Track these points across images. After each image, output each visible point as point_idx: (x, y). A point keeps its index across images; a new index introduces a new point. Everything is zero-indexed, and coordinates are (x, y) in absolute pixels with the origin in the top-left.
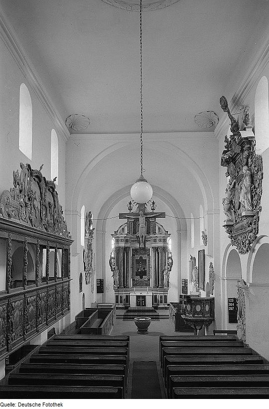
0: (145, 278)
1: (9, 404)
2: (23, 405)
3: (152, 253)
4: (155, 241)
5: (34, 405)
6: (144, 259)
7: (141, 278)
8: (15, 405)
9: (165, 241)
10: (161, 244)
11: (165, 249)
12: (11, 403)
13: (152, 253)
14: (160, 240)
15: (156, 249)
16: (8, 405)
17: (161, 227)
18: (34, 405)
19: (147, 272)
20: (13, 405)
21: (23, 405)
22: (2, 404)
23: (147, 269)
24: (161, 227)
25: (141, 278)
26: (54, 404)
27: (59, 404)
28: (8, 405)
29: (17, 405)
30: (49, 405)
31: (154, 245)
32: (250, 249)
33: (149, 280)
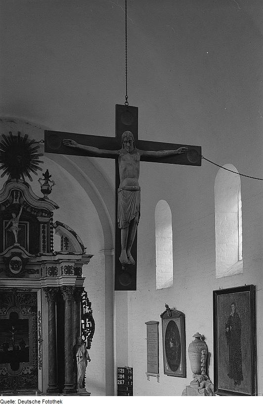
0: (25, 368)
1: (8, 401)
2: (23, 402)
3: (43, 306)
5: (33, 402)
6: (22, 317)
7: (15, 367)
8: (15, 402)
9: (78, 272)
11: (77, 292)
12: (11, 400)
13: (43, 306)
14: (68, 270)
15: (56, 295)
16: (8, 402)
17: (71, 236)
18: (33, 402)
19: (30, 352)
20: (13, 402)
21: (23, 402)
22: (2, 401)
23: (30, 345)
24: (71, 236)
26: (54, 401)
27: (58, 401)
28: (8, 402)
29: (17, 402)
30: (48, 402)
31: (48, 282)
32: (56, 267)
33: (35, 372)
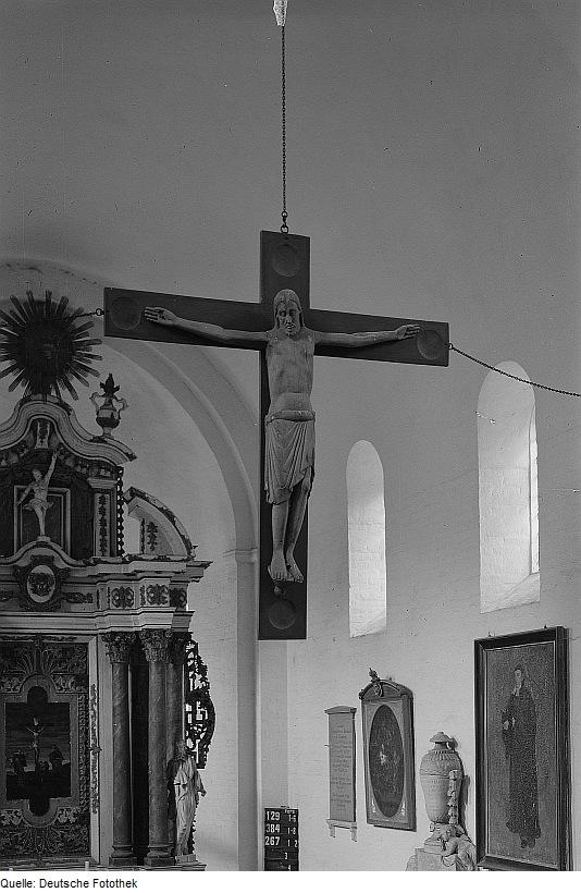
0: (62, 810)
1: (19, 883)
2: (50, 884)
3: (102, 674)
4: (124, 599)
5: (74, 884)
6: (54, 698)
7: (40, 808)
8: (34, 884)
10: (158, 619)
11: (177, 644)
12: (24, 880)
13: (102, 674)
14: (157, 595)
15: (130, 650)
16: (18, 884)
17: (161, 520)
18: (74, 884)
20: (28, 884)
21: (50, 884)
22: (4, 883)
23: (72, 758)
24: (161, 520)
25: (40, 808)
26: (118, 883)
27: (128, 883)
28: (18, 884)
29: (37, 884)
30: (106, 884)
31: (115, 622)
33: (84, 819)
